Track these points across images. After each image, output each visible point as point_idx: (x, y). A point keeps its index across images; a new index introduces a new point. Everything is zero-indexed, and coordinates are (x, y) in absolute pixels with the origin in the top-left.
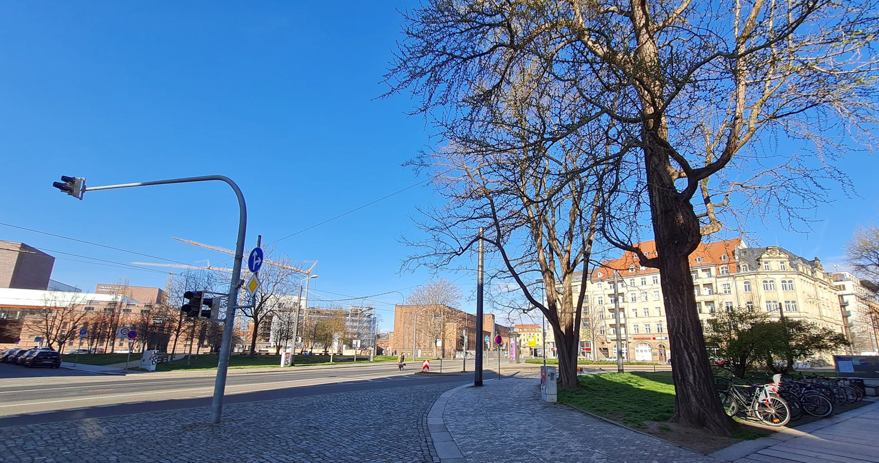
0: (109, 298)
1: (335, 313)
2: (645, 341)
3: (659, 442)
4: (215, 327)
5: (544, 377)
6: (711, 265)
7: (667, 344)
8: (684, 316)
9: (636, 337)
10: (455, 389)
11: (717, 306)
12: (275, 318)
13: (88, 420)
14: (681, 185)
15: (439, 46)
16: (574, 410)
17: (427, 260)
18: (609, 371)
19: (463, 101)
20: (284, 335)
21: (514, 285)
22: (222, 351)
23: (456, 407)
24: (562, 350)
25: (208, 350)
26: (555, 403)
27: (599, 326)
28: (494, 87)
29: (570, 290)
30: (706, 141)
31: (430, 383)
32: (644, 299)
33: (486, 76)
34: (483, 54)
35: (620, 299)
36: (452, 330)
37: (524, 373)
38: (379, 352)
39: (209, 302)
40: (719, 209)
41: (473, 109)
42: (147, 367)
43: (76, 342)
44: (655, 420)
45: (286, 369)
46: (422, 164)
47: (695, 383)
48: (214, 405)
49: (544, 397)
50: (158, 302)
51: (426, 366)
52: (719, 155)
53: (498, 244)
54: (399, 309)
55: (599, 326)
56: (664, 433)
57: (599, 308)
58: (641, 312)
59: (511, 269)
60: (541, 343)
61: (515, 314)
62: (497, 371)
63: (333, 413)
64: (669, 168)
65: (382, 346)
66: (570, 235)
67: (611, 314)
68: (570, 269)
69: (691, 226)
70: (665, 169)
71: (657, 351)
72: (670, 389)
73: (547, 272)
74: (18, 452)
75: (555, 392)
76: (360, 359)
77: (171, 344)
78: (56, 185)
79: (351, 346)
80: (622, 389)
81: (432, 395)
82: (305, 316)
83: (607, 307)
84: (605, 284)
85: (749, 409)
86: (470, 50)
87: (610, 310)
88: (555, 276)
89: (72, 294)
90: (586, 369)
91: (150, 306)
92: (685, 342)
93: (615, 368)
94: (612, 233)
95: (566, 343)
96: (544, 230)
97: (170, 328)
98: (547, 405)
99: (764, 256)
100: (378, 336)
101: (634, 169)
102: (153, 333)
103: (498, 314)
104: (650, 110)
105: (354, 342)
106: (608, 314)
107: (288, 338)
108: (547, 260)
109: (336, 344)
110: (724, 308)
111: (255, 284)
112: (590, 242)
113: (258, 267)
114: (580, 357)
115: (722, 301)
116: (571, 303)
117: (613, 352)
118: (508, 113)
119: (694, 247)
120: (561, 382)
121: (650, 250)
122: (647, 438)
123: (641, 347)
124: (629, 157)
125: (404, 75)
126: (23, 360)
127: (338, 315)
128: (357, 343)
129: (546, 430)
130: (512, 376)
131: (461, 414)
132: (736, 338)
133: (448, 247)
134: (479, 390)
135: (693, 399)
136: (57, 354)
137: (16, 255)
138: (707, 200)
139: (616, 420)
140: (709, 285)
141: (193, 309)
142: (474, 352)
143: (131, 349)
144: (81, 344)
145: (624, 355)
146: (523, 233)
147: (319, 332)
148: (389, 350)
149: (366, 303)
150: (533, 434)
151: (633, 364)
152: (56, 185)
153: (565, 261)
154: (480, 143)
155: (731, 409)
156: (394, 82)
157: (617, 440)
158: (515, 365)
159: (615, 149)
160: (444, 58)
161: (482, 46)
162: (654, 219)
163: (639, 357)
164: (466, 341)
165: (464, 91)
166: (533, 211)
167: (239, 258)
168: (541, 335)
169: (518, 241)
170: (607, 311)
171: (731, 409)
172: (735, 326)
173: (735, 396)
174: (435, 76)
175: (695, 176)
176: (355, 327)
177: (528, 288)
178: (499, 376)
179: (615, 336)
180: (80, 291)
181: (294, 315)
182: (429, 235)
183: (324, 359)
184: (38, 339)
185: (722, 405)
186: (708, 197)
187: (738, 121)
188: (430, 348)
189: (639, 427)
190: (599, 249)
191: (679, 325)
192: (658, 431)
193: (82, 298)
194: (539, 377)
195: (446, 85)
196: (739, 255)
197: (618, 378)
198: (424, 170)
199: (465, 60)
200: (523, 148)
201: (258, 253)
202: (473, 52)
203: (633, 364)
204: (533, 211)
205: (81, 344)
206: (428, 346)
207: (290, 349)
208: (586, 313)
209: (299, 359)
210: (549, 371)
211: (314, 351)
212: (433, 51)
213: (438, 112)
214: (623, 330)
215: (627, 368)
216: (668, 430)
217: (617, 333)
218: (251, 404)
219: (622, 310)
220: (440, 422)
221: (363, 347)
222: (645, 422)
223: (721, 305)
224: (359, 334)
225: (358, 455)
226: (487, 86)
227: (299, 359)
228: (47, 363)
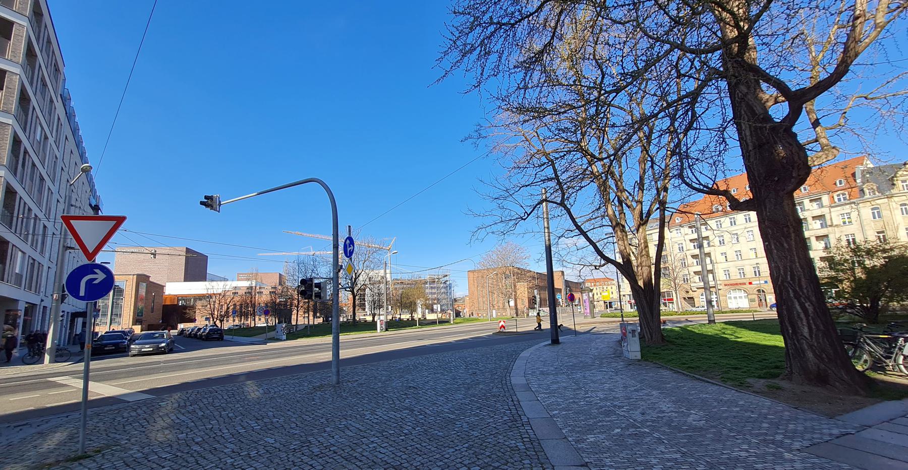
0: (246, 284)
1: (416, 282)
2: (738, 287)
3: (768, 402)
4: (324, 303)
5: (624, 334)
6: (824, 193)
7: (769, 287)
8: (792, 262)
9: (727, 282)
10: (533, 348)
11: (833, 241)
12: (367, 290)
13: (249, 382)
14: (779, 111)
15: (486, 18)
16: (662, 367)
17: (494, 228)
18: (698, 322)
19: (515, 67)
20: (377, 305)
21: (582, 241)
22: (331, 323)
23: (537, 366)
24: (644, 314)
25: (320, 320)
26: (639, 360)
27: (680, 275)
28: (545, 46)
29: (646, 242)
30: (810, 52)
31: (506, 343)
32: (734, 241)
33: (535, 36)
34: (531, 14)
35: (705, 243)
36: (523, 290)
37: (600, 328)
38: (458, 314)
39: (318, 285)
40: (833, 131)
41: (526, 73)
42: (280, 337)
43: (231, 319)
44: (760, 377)
45: (383, 333)
46: (480, 136)
47: (811, 337)
48: (334, 370)
49: (626, 354)
50: (280, 284)
51: (502, 326)
52: (831, 69)
53: (562, 204)
54: (471, 274)
55: (680, 275)
56: (773, 392)
57: (680, 255)
58: (731, 255)
59: (578, 227)
60: (616, 296)
61: (586, 271)
62: (573, 327)
63: (426, 374)
64: (761, 95)
65: (459, 309)
66: (641, 185)
67: (695, 261)
68: (643, 220)
69: (796, 158)
70: (756, 97)
71: (755, 297)
72: (778, 341)
73: (618, 226)
74: (211, 408)
75: (638, 349)
76: (442, 322)
77: (294, 317)
78: (202, 203)
79: (432, 311)
80: (716, 343)
81: (512, 355)
82: (391, 287)
83: (688, 253)
84: (686, 230)
85: (890, 363)
86: (517, 13)
87: (694, 256)
88: (627, 228)
89: (223, 283)
90: (670, 321)
91: (275, 288)
92: (795, 291)
93: (704, 319)
94: (695, 180)
95: (646, 298)
96: (611, 182)
97: (291, 305)
98: (630, 363)
99: (900, 173)
100: (455, 300)
101: (716, 107)
102: (280, 309)
103: (567, 271)
104: (732, 33)
105: (435, 307)
106: (690, 260)
107: (380, 307)
108: (617, 213)
109: (419, 310)
110: (844, 243)
111: (351, 267)
112: (666, 189)
113: (351, 253)
114: (662, 308)
115: (838, 236)
116: (648, 255)
117: (701, 301)
118: (561, 68)
119: (802, 181)
120: (644, 337)
121: (742, 190)
122: (753, 399)
123: (733, 294)
124: (710, 92)
125: (455, 55)
126: (201, 335)
127: (418, 285)
128: (437, 307)
129: (633, 389)
130: (588, 332)
131: (542, 373)
132: (863, 277)
133: (513, 213)
134: (557, 348)
135: (810, 355)
136: (220, 330)
137: (183, 260)
138: (816, 124)
139: (712, 378)
140: (821, 217)
141: (308, 293)
142: (547, 309)
143: (267, 323)
144: (234, 321)
145: (714, 303)
146: (591, 190)
147: (404, 300)
148: (466, 312)
149: (441, 273)
150: (620, 394)
151: (726, 312)
152: (202, 203)
153: (637, 212)
154: (534, 109)
155: (862, 362)
156: (447, 64)
157: (716, 400)
158: (590, 320)
159: (692, 85)
160: (492, 29)
161: (529, 6)
162: (746, 156)
163: (732, 304)
164: (538, 300)
165: (517, 57)
166: (598, 167)
167: (336, 247)
168: (615, 288)
169: (585, 200)
170: (689, 257)
171: (862, 362)
172: (861, 263)
173: (867, 348)
174: (485, 50)
175: (798, 100)
176: (434, 293)
177: (598, 244)
178: (575, 333)
179: (702, 284)
180: (227, 280)
181: (382, 286)
182: (494, 205)
183: (411, 323)
184: (207, 319)
185: (850, 358)
186: (817, 120)
187: (859, 21)
188: (504, 308)
189: (741, 385)
190: (675, 195)
191: (785, 273)
192: (766, 390)
193: (230, 285)
194: (618, 331)
195: (496, 55)
196: (863, 176)
197: (710, 330)
198: (482, 142)
199: (513, 25)
200: (583, 106)
201: (350, 241)
202: (521, 14)
203: (726, 312)
204: (598, 167)
205: (234, 321)
206: (501, 306)
207: (382, 318)
208: (665, 263)
209: (392, 325)
210: (629, 328)
211: (403, 317)
212: (480, 25)
213: (493, 85)
214: (710, 276)
215: (718, 318)
216: (778, 388)
217: (704, 279)
218: (360, 366)
219: (709, 255)
220: (522, 381)
221: (442, 311)
222: (748, 380)
223: (839, 240)
224: (438, 300)
225: (453, 413)
226: (537, 47)
227: (392, 325)
228: (215, 337)
